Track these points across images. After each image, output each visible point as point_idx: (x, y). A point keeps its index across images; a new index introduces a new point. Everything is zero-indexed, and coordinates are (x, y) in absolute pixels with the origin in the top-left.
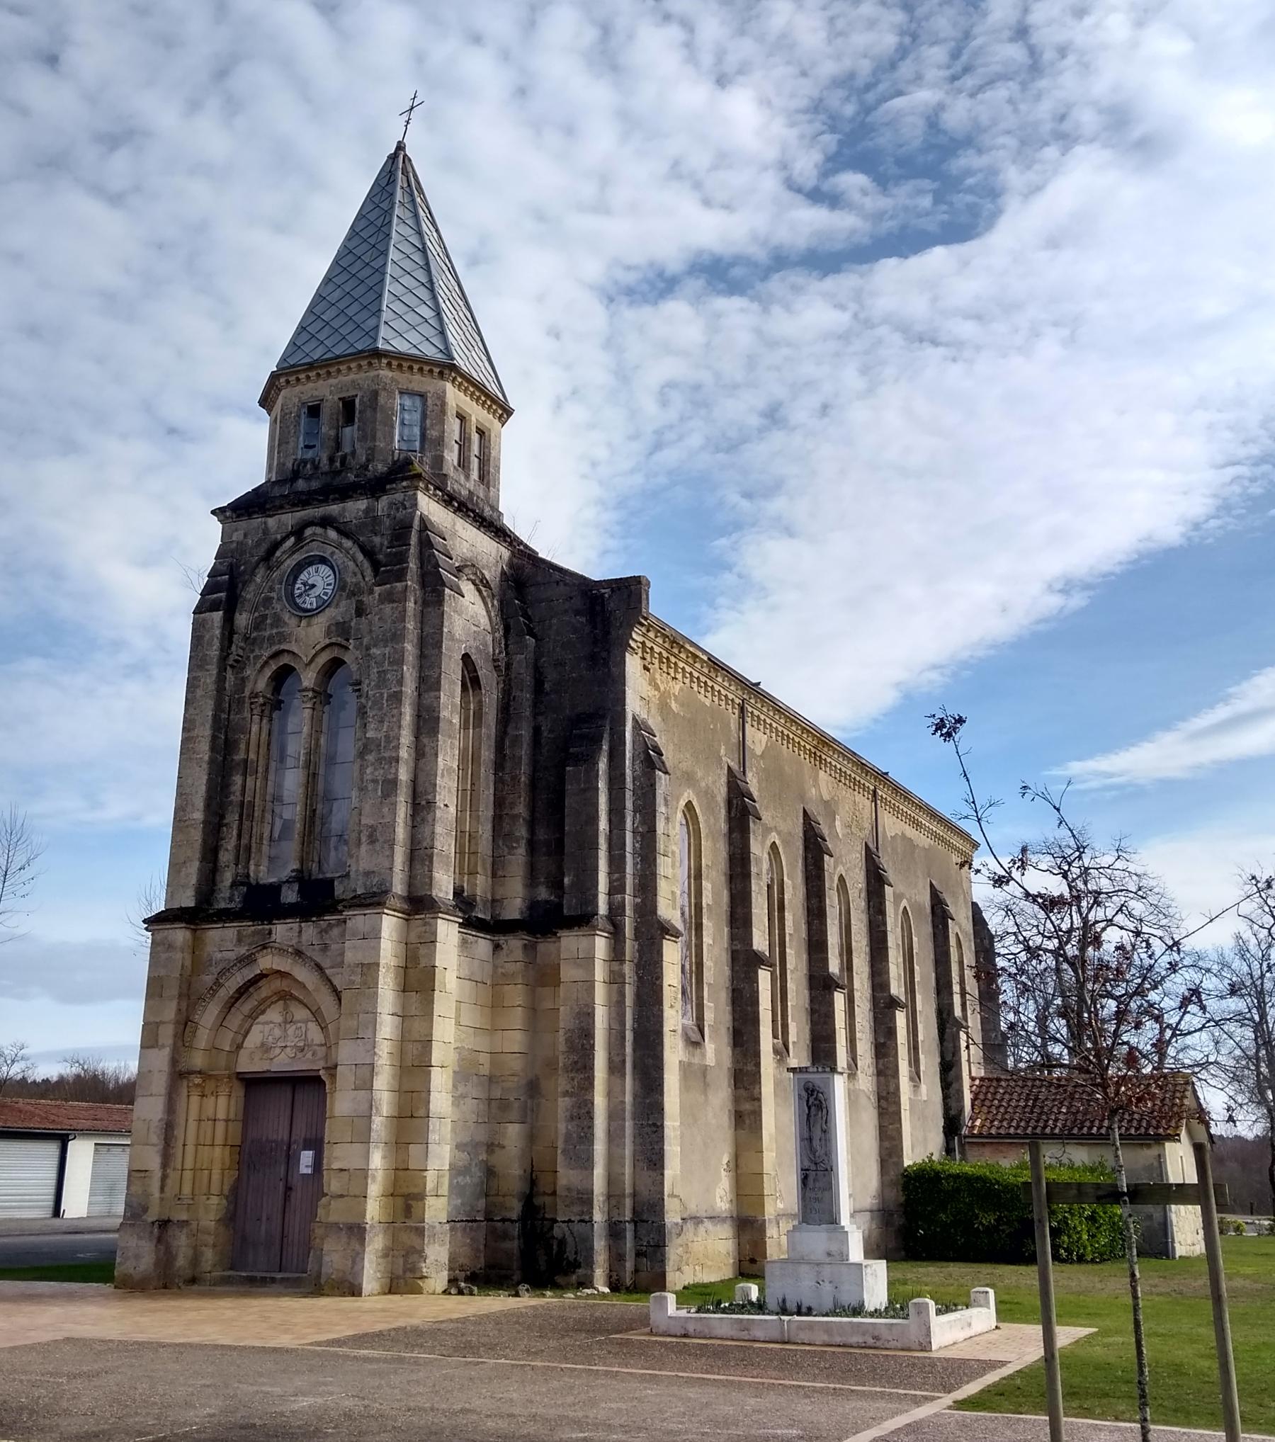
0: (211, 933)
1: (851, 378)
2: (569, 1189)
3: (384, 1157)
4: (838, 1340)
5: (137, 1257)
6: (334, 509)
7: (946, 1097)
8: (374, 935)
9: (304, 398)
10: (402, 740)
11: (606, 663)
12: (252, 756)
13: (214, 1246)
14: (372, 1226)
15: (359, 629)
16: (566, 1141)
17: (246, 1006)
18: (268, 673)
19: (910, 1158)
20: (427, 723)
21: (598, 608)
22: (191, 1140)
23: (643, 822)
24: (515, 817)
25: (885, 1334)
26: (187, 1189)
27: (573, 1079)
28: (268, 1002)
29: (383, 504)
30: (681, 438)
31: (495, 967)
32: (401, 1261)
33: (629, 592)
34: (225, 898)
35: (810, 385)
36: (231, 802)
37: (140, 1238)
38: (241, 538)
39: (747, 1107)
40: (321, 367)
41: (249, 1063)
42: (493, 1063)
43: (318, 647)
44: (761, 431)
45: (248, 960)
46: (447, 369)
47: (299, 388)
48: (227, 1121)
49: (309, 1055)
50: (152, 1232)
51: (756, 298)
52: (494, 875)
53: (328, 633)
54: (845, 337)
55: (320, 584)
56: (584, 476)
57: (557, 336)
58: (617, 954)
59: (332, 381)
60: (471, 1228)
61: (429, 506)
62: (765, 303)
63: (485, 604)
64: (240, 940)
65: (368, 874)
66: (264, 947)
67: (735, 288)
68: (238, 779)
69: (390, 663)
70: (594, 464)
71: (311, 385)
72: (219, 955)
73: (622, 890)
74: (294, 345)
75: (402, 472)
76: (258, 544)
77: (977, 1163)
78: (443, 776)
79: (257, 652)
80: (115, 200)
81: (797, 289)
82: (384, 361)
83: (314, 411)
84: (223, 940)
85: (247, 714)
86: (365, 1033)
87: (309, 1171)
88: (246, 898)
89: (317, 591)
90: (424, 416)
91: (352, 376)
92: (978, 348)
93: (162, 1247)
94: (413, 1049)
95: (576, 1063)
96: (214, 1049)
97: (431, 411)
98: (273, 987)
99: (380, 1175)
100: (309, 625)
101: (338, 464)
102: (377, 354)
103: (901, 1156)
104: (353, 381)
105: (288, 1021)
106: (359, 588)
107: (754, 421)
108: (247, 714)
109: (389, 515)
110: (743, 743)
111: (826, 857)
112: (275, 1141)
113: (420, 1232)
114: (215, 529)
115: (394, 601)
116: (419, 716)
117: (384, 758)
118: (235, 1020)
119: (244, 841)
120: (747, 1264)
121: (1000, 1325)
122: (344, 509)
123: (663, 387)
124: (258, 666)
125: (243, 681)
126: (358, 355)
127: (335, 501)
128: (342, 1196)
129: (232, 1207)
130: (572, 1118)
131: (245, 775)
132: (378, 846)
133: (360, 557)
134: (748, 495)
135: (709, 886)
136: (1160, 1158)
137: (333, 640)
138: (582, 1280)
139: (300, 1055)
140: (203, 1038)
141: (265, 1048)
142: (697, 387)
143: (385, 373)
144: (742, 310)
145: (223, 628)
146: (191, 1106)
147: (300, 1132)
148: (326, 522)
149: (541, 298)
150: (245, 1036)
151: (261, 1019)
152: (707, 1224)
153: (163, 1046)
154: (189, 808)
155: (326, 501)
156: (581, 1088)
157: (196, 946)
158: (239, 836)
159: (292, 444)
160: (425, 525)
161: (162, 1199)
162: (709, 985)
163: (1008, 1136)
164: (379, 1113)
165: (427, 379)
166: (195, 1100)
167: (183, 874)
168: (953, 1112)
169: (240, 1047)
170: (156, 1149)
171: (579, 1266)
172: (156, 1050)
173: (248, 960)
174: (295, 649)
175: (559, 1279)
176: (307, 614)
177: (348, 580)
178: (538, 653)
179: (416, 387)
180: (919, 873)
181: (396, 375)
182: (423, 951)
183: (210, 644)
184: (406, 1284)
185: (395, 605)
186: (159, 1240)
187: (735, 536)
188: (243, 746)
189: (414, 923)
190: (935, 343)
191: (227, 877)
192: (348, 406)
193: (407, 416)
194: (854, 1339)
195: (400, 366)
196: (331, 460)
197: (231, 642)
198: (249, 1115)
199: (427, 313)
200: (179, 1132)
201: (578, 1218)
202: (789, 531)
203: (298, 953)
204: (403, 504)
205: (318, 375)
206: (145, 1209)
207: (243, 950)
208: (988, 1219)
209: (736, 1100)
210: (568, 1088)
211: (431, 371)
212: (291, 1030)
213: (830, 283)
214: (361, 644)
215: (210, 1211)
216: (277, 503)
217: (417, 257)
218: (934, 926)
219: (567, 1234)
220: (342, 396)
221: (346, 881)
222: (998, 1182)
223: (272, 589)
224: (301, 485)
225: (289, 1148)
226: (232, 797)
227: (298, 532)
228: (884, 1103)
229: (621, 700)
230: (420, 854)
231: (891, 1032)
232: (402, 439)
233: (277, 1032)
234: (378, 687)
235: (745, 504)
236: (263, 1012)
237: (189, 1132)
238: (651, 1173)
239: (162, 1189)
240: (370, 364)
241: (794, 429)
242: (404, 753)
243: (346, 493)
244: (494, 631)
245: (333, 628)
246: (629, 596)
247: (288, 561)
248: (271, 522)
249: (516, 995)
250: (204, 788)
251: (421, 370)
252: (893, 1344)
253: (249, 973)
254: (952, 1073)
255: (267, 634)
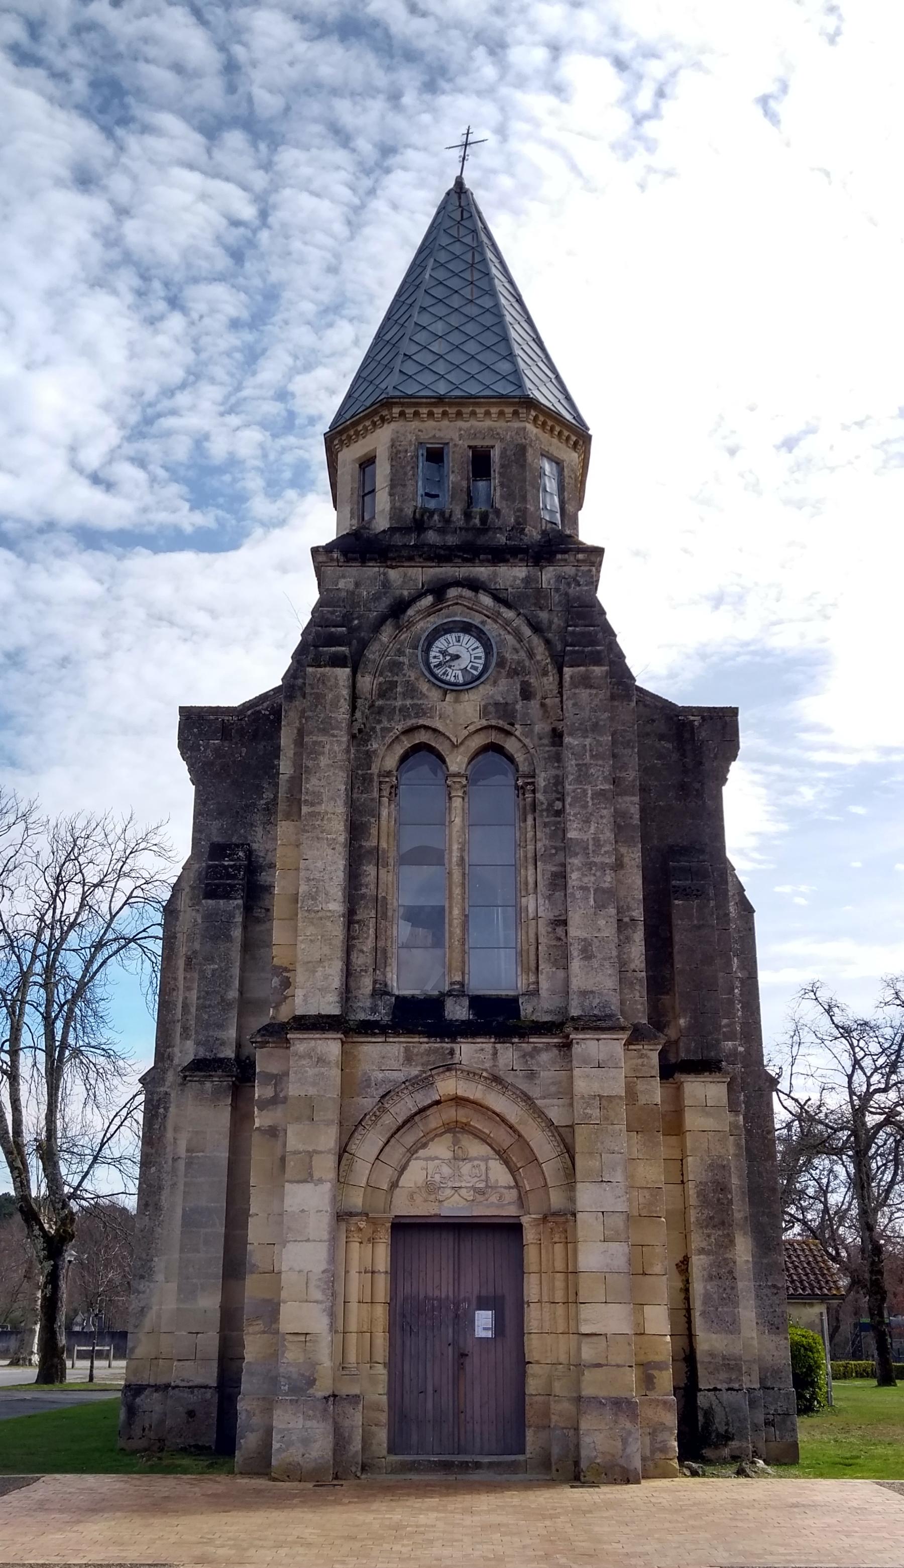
0: (366, 1048)
2: (712, 1355)
5: (306, 1442)
6: (482, 572)
9: (424, 437)
11: (699, 794)
12: (383, 845)
15: (527, 714)
16: (705, 1303)
17: (409, 1138)
21: (687, 735)
27: (709, 1236)
28: (432, 1135)
29: (548, 576)
32: (647, 1440)
36: (363, 896)
37: (308, 1417)
38: (351, 587)
40: (451, 405)
41: (406, 1206)
43: (472, 728)
47: (415, 424)
49: (494, 1199)
50: (325, 1410)
53: (484, 712)
54: (91, 604)
59: (460, 424)
62: (29, 559)
64: (409, 1059)
65: (584, 994)
66: (449, 1068)
69: (592, 756)
71: (431, 423)
72: (380, 1075)
76: (376, 598)
79: (386, 724)
82: (533, 413)
83: (436, 456)
87: (489, 1334)
89: (464, 662)
91: (488, 423)
92: (206, 635)
95: (711, 1218)
98: (444, 1117)
100: (457, 701)
101: (477, 521)
104: (491, 429)
105: (458, 1158)
106: (524, 667)
109: (557, 590)
112: (440, 1300)
115: (591, 687)
117: (595, 864)
118: (395, 1154)
122: (495, 574)
124: (388, 740)
126: (503, 399)
127: (482, 563)
128: (599, 1365)
130: (711, 1278)
132: (595, 963)
133: (527, 632)
137: (493, 722)
138: (737, 1453)
139: (480, 1198)
140: (362, 1171)
141: (431, 1188)
147: (471, 1286)
148: (474, 585)
150: (401, 1173)
151: (421, 1153)
153: (320, 1181)
154: (321, 897)
155: (470, 561)
156: (720, 1246)
157: (347, 1061)
159: (410, 489)
165: (563, 446)
167: (319, 974)
170: (323, 1306)
171: (732, 1439)
172: (310, 1186)
173: (423, 1082)
174: (438, 724)
175: (707, 1452)
177: (508, 656)
183: (335, 704)
184: (656, 1467)
185: (594, 691)
188: (374, 831)
190: (172, 623)
191: (366, 984)
196: (468, 515)
198: (397, 1270)
201: (724, 1386)
203: (496, 1079)
204: (575, 579)
205: (445, 413)
206: (312, 1382)
207: (415, 1071)
210: (704, 1244)
212: (466, 1168)
213: (89, 557)
214: (532, 731)
216: (405, 553)
219: (715, 1402)
220: (473, 443)
221: (535, 1000)
223: (400, 652)
224: (432, 537)
225: (457, 1307)
226: (364, 890)
227: (438, 590)
233: (446, 1170)
234: (578, 780)
236: (424, 1146)
238: (774, 1337)
240: (516, 413)
241: (32, 673)
243: (500, 555)
245: (491, 709)
246: (724, 728)
247: (422, 624)
250: (341, 874)
253: (423, 1099)
255: (399, 703)
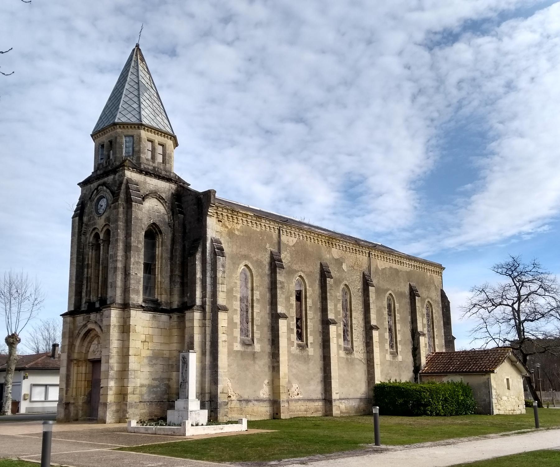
0: (78, 318)
1: (543, 63)
3: (115, 383)
4: (166, 433)
6: (106, 179)
7: (415, 360)
8: (109, 316)
10: (119, 254)
12: (90, 262)
13: (82, 410)
14: (110, 404)
17: (88, 339)
18: (93, 235)
19: (377, 382)
20: (128, 248)
22: (75, 380)
23: (213, 274)
24: (175, 275)
25: (176, 431)
26: (74, 394)
30: (470, 103)
31: (170, 323)
33: (209, 194)
34: (84, 307)
35: (525, 70)
39: (276, 364)
42: (170, 354)
44: (506, 93)
45: (85, 325)
46: (140, 125)
48: (86, 374)
51: (496, 35)
52: (171, 295)
55: (104, 205)
56: (428, 126)
57: (409, 68)
58: (204, 318)
59: (106, 135)
60: (160, 404)
61: (130, 174)
63: (163, 205)
66: (88, 322)
67: (484, 33)
68: (86, 270)
70: (432, 120)
73: (206, 297)
74: (98, 124)
75: (122, 165)
77: (425, 383)
78: (134, 264)
80: (229, 44)
81: (514, 28)
84: (80, 319)
85: (87, 249)
86: (107, 346)
88: (88, 306)
90: (133, 143)
93: (67, 410)
94: (125, 350)
96: (80, 353)
97: (136, 141)
99: (114, 389)
102: (115, 124)
103: (374, 380)
107: (501, 90)
108: (87, 249)
110: (279, 242)
111: (328, 279)
113: (126, 405)
114: (79, 189)
116: (126, 246)
118: (86, 344)
119: (88, 289)
120: (275, 415)
121: (249, 430)
123: (458, 83)
125: (86, 238)
129: (89, 399)
131: (88, 268)
134: (501, 122)
135: (258, 293)
136: (489, 380)
140: (77, 350)
141: (94, 352)
142: (474, 79)
143: (119, 130)
144: (489, 42)
145: (79, 222)
146: (74, 369)
148: (104, 184)
149: (400, 53)
152: (256, 403)
155: (103, 177)
158: (87, 288)
160: (129, 181)
161: (66, 397)
162: (257, 325)
163: (435, 373)
164: (112, 369)
165: (134, 130)
166: (76, 367)
168: (417, 365)
169: (88, 351)
173: (85, 325)
176: (100, 215)
178: (184, 220)
179: (130, 134)
180: (402, 280)
181: (123, 130)
182: (127, 320)
186: (66, 408)
187: (498, 141)
189: (126, 312)
192: (111, 142)
193: (127, 144)
194: (169, 433)
195: (124, 127)
196: (106, 163)
197: (82, 226)
199: (135, 106)
200: (72, 377)
202: (521, 135)
207: (84, 323)
208: (401, 401)
209: (273, 362)
211: (135, 127)
215: (81, 400)
217: (136, 87)
218: (411, 299)
222: (403, 388)
223: (92, 208)
228: (369, 362)
229: (205, 233)
230: (126, 290)
231: (371, 338)
232: (126, 153)
235: (500, 127)
237: (74, 377)
239: (66, 394)
242: (119, 258)
244: (168, 214)
248: (92, 185)
249: (175, 332)
251: (131, 127)
252: (178, 434)
254: (417, 352)
